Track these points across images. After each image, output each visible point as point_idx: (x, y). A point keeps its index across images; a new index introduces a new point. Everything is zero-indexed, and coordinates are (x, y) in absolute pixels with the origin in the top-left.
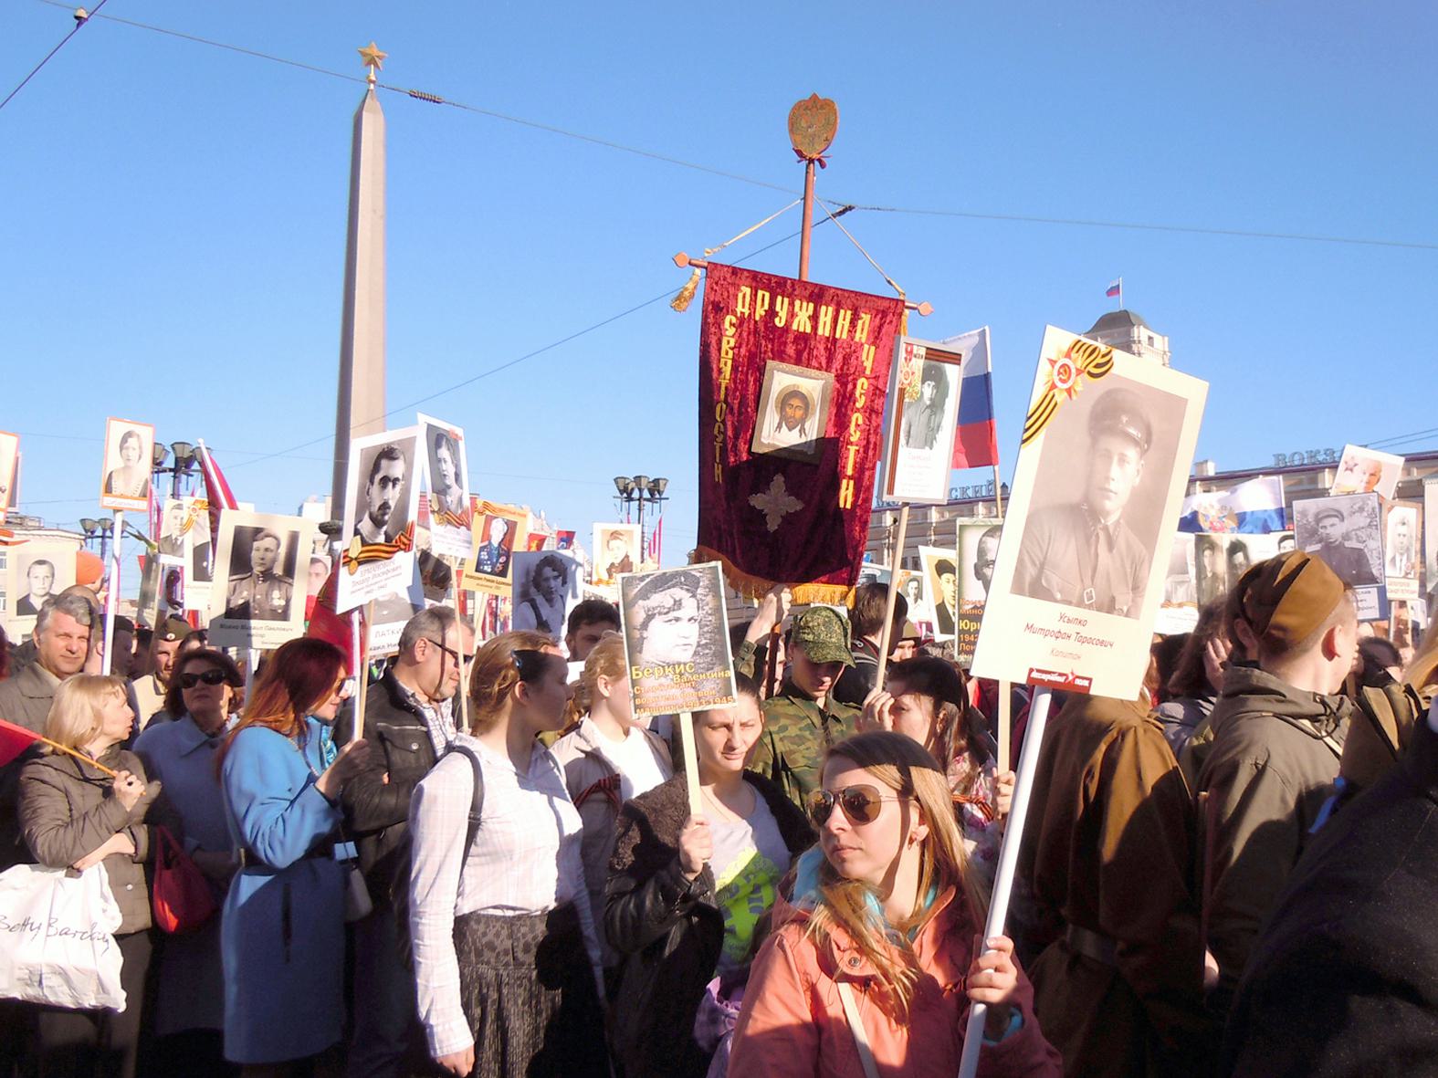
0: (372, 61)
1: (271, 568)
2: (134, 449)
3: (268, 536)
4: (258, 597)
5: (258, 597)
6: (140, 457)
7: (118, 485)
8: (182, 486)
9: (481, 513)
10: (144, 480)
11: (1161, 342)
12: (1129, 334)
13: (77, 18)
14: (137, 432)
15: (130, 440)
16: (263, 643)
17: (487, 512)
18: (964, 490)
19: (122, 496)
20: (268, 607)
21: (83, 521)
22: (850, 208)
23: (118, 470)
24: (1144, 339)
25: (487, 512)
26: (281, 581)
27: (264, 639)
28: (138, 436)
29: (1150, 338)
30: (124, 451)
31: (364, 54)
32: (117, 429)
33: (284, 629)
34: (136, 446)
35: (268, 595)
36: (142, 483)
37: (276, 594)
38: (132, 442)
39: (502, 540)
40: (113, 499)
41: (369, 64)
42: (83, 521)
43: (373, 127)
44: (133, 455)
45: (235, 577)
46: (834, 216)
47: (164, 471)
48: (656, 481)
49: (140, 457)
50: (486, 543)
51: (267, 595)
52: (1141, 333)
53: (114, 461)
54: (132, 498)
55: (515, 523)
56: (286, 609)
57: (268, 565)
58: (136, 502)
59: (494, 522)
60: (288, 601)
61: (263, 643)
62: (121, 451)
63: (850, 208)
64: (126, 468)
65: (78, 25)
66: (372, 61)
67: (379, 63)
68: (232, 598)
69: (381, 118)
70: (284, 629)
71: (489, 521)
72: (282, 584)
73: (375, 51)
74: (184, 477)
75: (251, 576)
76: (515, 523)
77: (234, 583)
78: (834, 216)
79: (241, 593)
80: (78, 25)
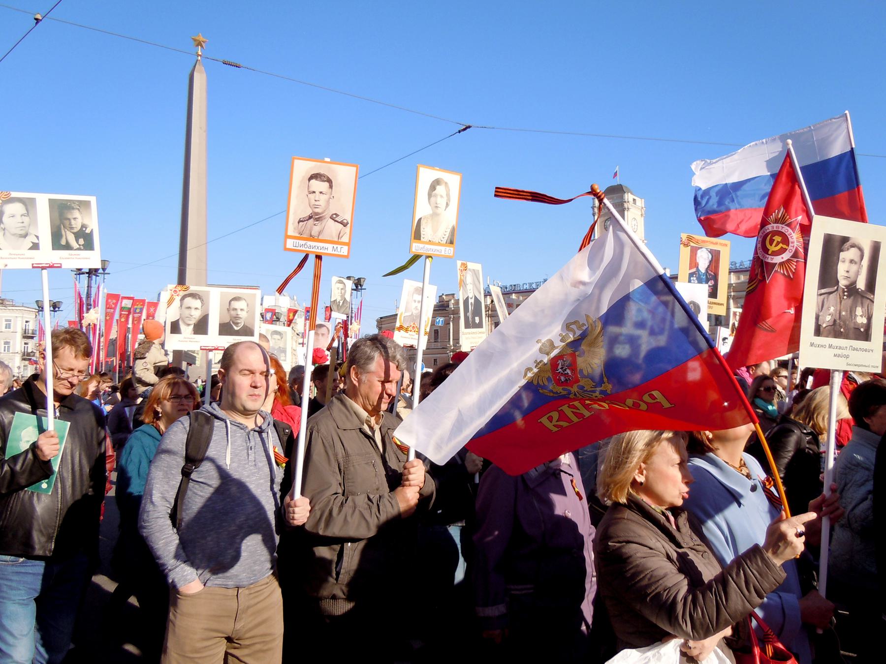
0: (199, 44)
1: (855, 283)
2: (442, 196)
3: (853, 246)
4: (844, 313)
5: (844, 313)
6: (447, 205)
7: (427, 232)
8: (93, 282)
9: (686, 245)
10: (451, 227)
11: (640, 202)
12: (622, 197)
13: (36, 19)
14: (446, 180)
15: (438, 187)
16: (848, 364)
17: (692, 244)
18: (531, 284)
19: (430, 242)
20: (852, 325)
21: (37, 302)
22: (469, 127)
23: (425, 217)
24: (631, 200)
25: (692, 244)
26: (863, 297)
27: (849, 361)
28: (446, 183)
29: (634, 200)
30: (432, 199)
31: (195, 40)
32: (426, 175)
33: (866, 350)
34: (444, 194)
35: (852, 311)
36: (449, 231)
37: (859, 311)
38: (440, 189)
39: (709, 266)
40: (421, 246)
41: (197, 45)
42: (37, 302)
43: (200, 80)
44: (442, 202)
45: (823, 291)
46: (459, 132)
47: (83, 273)
48: (359, 279)
49: (447, 205)
50: (694, 270)
51: (851, 312)
52: (628, 197)
53: (422, 208)
54: (439, 244)
55: (719, 252)
56: (868, 326)
57: (852, 279)
58: (443, 248)
59: (699, 252)
60: (869, 319)
61: (848, 364)
62: (429, 199)
63: (469, 127)
64: (435, 215)
65: (37, 23)
66: (199, 44)
67: (204, 45)
68: (821, 314)
69: (204, 75)
70: (866, 350)
71: (694, 252)
72: (865, 300)
73: (201, 38)
74: (94, 277)
75: (837, 290)
76: (719, 252)
77: (822, 297)
78: (459, 132)
79: (828, 309)
80: (37, 23)
